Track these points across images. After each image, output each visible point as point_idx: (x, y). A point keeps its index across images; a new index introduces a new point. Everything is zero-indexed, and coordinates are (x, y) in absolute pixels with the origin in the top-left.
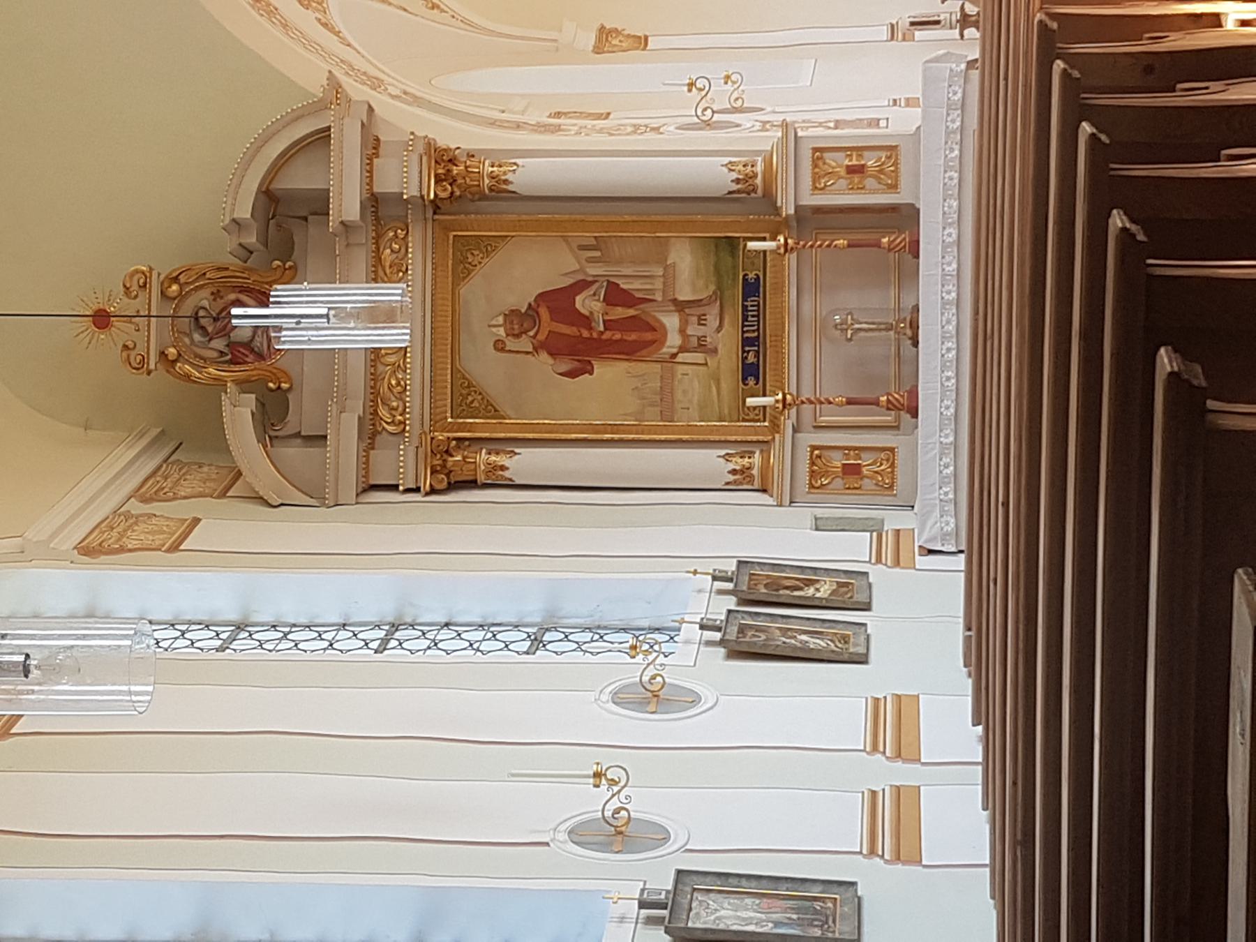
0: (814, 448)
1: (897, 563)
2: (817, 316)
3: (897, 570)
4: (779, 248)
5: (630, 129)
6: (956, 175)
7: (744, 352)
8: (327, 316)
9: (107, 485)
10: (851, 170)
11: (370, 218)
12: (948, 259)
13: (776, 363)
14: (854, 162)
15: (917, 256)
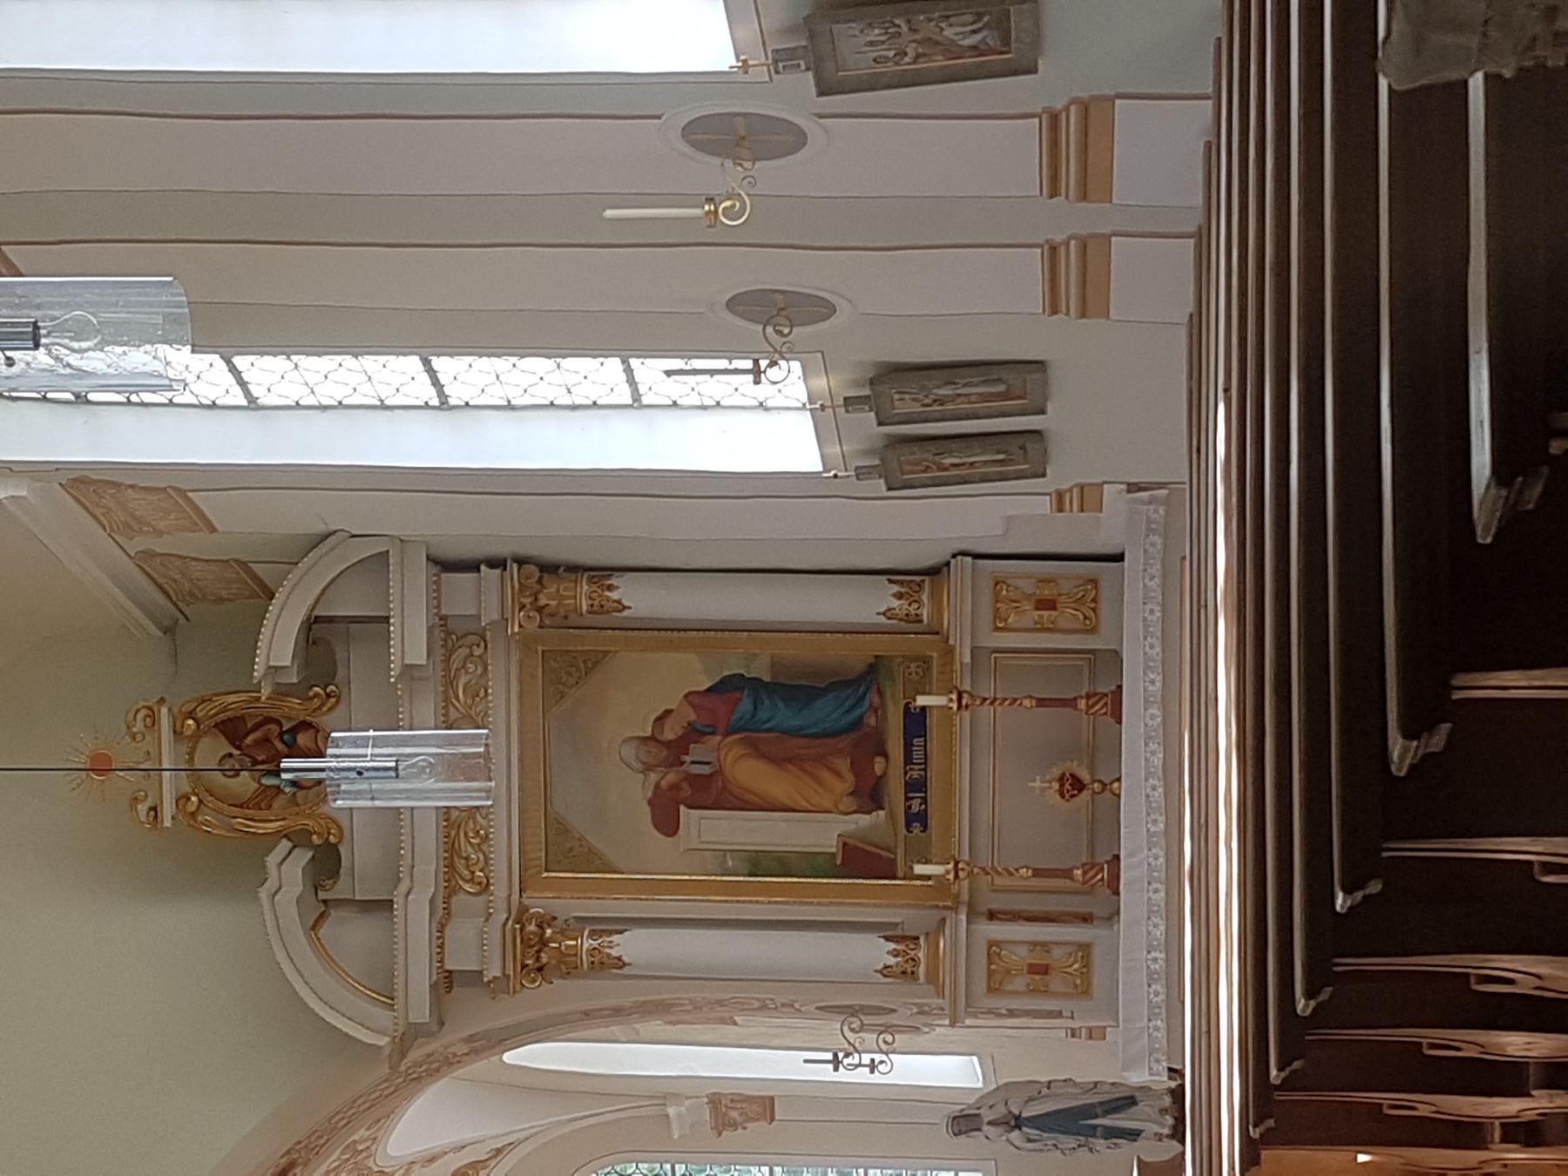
0: (991, 944)
1: (1084, 197)
2: (991, 786)
3: (1084, 204)
4: (948, 872)
5: (757, 1004)
6: (1162, 853)
7: (907, 799)
8: (396, 769)
9: (148, 574)
10: (1034, 969)
11: (439, 654)
12: (1152, 746)
13: (945, 664)
14: (1046, 613)
15: (1120, 723)
